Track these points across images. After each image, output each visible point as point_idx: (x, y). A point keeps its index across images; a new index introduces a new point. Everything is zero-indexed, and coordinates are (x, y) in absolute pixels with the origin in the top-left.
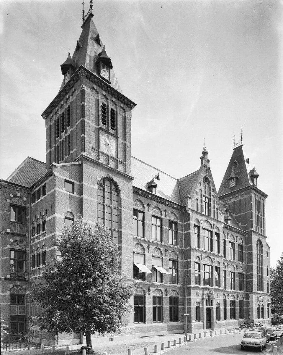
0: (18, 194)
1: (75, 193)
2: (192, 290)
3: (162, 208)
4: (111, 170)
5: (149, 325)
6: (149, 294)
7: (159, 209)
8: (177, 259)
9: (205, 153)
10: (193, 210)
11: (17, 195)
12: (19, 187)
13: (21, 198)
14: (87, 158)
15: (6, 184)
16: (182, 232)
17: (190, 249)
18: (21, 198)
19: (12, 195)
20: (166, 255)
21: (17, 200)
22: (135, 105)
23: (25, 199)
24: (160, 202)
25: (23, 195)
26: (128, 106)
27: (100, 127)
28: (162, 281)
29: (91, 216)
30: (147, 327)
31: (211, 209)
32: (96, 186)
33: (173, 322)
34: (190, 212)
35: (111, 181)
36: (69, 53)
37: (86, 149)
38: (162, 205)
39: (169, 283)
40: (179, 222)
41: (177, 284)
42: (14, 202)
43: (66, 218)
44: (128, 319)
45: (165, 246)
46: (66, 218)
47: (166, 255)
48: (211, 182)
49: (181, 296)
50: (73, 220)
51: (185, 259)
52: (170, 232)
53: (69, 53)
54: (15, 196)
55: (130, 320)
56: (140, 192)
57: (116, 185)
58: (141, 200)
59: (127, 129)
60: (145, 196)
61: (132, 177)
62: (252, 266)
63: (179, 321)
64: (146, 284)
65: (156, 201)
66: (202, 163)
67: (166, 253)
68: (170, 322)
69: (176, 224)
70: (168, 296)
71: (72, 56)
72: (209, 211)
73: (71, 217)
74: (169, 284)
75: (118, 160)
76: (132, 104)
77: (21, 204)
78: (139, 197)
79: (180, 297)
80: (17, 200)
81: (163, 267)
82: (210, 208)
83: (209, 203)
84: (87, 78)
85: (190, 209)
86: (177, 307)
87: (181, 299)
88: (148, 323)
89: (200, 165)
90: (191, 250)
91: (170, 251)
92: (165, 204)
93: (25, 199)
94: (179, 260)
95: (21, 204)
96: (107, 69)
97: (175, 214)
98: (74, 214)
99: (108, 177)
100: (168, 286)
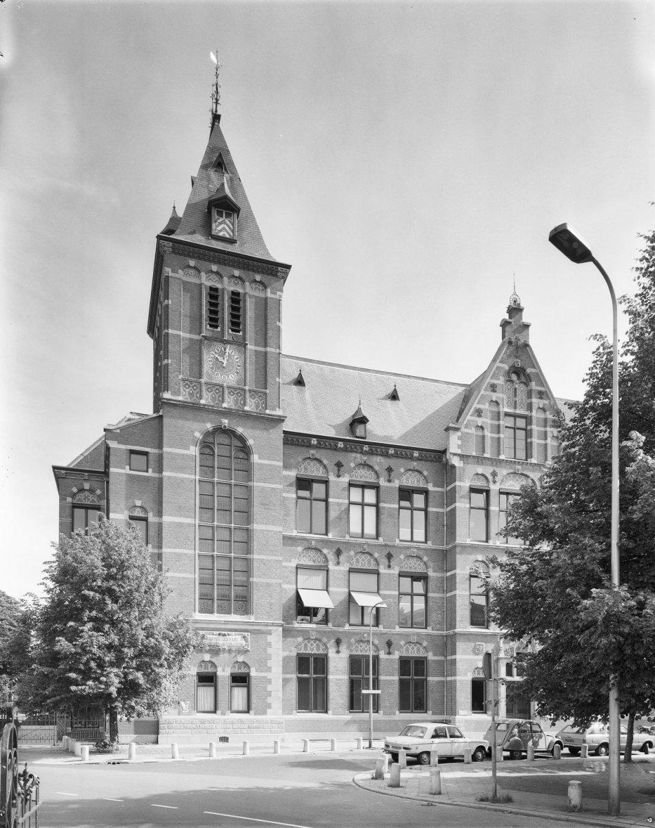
0: (87, 486)
1: (150, 470)
2: (457, 643)
3: (380, 464)
4: (227, 413)
5: (335, 716)
6: (338, 652)
7: (371, 467)
8: (425, 571)
9: (515, 310)
10: (467, 456)
11: (85, 488)
12: (86, 474)
13: (92, 491)
14: (172, 402)
15: (63, 472)
16: (441, 510)
17: (455, 547)
18: (92, 491)
19: (75, 490)
20: (389, 566)
21: (85, 495)
22: (289, 267)
23: (98, 492)
24: (371, 453)
25: (95, 485)
26: (273, 275)
27: (203, 336)
28: (377, 625)
29: (180, 507)
30: (332, 721)
31: (531, 443)
32: (194, 451)
33: (412, 712)
34: (456, 461)
35: (230, 433)
36: (174, 208)
37: (171, 385)
38: (380, 457)
39: (397, 627)
40: (431, 487)
41: (426, 628)
42: (79, 500)
43: (132, 518)
44: (268, 702)
45: (386, 545)
46: (132, 518)
47: (389, 566)
48: (532, 377)
49: (435, 655)
50: (145, 519)
51: (447, 571)
52: (405, 514)
53: (174, 208)
54: (81, 490)
55: (272, 705)
56: (314, 441)
57: (242, 439)
58: (318, 456)
59: (269, 321)
60: (329, 447)
61: (280, 416)
62: (212, 612)
63: (431, 712)
64: (329, 632)
65: (361, 453)
66: (504, 337)
67: (389, 561)
68: (400, 712)
69: (425, 492)
70: (396, 656)
71: (180, 214)
72: (528, 447)
73: (142, 515)
74: (398, 629)
75: (247, 388)
76: (279, 269)
77: (93, 501)
78: (312, 452)
79: (431, 657)
80: (85, 495)
81: (381, 592)
82: (529, 440)
83: (529, 428)
84: (174, 252)
85: (455, 454)
86: (426, 679)
87: (434, 661)
88: (333, 711)
89: (500, 341)
90: (458, 550)
91: (402, 557)
92: (386, 455)
93: (98, 492)
94: (431, 573)
95: (93, 501)
96: (228, 216)
97: (420, 472)
98: (148, 509)
99: (221, 428)
100: (393, 634)
